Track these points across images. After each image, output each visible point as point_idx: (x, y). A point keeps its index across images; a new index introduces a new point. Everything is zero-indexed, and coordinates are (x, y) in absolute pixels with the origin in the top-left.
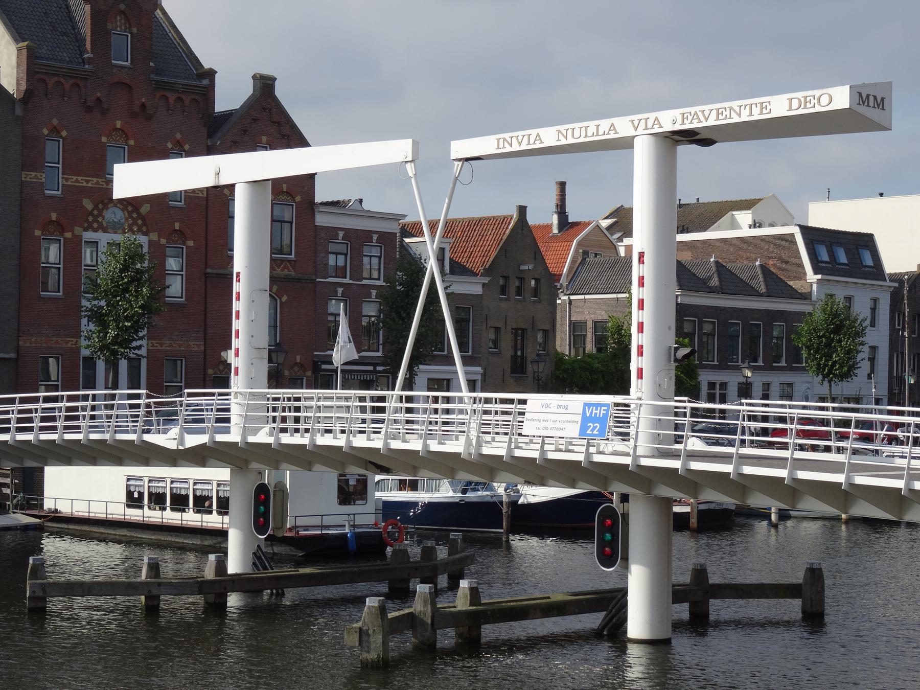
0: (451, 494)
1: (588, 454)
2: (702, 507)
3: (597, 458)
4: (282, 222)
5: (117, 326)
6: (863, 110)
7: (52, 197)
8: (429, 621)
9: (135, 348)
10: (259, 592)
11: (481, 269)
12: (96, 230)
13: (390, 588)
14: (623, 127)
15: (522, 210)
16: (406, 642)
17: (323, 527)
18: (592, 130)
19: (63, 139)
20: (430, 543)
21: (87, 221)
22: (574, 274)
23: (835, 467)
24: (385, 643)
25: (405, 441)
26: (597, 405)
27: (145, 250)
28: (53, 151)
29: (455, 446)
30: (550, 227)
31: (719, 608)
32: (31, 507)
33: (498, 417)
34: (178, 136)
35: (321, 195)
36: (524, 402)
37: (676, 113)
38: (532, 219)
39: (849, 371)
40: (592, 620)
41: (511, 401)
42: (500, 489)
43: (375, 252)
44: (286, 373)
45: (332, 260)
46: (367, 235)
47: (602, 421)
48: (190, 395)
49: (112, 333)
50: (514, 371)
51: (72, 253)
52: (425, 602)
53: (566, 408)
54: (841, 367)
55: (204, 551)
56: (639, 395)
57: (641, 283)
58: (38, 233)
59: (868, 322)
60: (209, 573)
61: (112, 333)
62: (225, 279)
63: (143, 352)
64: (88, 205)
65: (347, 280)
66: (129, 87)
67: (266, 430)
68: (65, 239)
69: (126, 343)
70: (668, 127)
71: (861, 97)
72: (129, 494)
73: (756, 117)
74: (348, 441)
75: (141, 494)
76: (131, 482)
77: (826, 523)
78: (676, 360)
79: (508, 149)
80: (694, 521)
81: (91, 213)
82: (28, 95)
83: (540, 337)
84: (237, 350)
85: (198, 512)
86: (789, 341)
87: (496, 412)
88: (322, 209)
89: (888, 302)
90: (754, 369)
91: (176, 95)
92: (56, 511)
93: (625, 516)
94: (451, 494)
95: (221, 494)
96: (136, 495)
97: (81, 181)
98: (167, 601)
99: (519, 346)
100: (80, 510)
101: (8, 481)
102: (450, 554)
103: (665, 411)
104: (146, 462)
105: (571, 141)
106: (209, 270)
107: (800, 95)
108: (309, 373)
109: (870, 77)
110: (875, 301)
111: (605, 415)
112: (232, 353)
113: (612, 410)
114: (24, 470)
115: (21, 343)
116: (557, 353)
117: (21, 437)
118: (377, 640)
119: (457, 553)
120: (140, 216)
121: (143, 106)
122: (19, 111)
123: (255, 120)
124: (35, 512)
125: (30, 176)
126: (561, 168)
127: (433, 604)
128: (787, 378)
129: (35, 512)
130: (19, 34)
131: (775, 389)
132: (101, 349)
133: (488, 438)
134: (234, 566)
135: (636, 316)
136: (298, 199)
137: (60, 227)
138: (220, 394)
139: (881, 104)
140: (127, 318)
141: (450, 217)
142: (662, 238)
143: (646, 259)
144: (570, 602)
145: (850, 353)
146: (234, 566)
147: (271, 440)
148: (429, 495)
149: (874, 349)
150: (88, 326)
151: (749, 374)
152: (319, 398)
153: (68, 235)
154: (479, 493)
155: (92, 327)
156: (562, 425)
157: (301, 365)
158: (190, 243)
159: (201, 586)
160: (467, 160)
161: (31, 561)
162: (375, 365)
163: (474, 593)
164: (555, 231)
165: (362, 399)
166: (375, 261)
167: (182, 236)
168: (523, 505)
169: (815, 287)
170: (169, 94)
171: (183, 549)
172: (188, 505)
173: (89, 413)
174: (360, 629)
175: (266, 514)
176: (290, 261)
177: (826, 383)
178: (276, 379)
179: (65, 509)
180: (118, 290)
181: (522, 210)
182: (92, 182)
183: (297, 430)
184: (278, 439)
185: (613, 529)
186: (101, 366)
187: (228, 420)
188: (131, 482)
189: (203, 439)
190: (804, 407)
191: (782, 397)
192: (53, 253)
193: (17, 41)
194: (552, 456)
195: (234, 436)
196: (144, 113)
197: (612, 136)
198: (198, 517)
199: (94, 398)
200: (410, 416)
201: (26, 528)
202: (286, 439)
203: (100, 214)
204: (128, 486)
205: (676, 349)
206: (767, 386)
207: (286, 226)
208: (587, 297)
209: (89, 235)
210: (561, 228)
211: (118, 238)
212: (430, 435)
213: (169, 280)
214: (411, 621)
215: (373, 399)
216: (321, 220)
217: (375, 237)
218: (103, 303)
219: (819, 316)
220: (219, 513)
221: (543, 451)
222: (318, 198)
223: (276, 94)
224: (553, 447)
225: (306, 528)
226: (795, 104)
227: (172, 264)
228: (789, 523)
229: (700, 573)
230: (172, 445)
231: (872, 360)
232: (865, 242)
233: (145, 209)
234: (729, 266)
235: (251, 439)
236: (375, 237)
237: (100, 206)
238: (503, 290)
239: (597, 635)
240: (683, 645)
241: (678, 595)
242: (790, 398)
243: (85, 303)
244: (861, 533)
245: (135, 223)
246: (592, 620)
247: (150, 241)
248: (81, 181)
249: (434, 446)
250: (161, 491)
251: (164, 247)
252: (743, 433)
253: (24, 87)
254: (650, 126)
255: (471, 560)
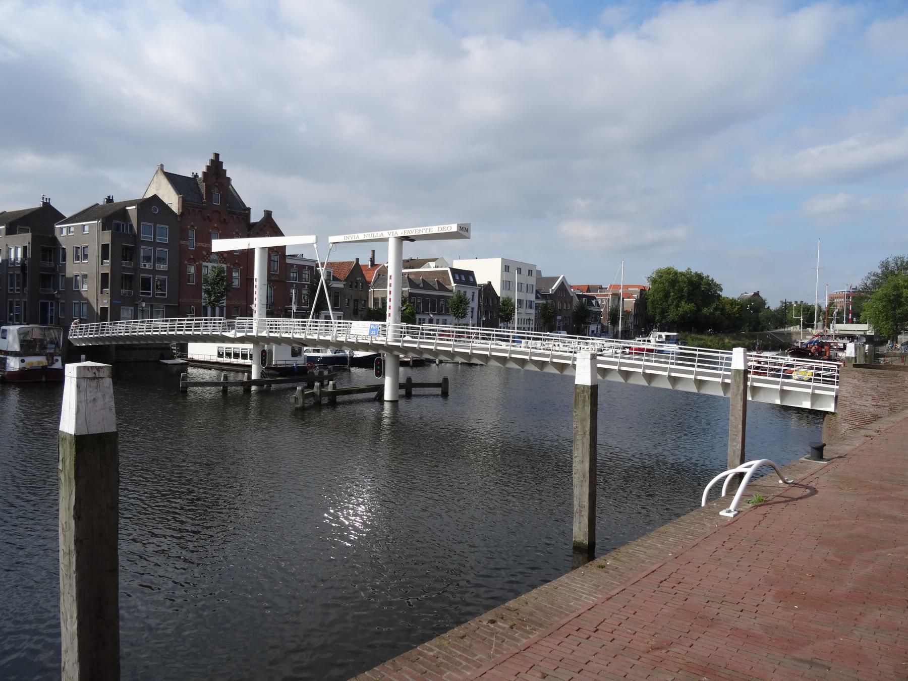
0: (331, 354)
1: (372, 341)
2: (414, 359)
3: (374, 342)
4: (274, 261)
5: (215, 296)
6: (461, 232)
7: (191, 250)
8: (319, 394)
9: (221, 303)
10: (263, 386)
11: (343, 279)
12: (207, 262)
13: (308, 384)
14: (385, 234)
15: (357, 260)
16: (312, 401)
17: (286, 364)
18: (375, 235)
19: (196, 230)
20: (321, 370)
21: (204, 259)
22: (375, 281)
23: (449, 346)
24: (303, 402)
25: (312, 336)
26: (374, 325)
27: (225, 269)
28: (192, 234)
29: (328, 338)
30: (368, 265)
31: (414, 391)
32: (183, 357)
33: (343, 328)
34: (237, 230)
35: (287, 253)
36: (351, 323)
37: (403, 230)
38: (361, 263)
39: (464, 315)
40: (373, 395)
41: (347, 323)
42: (347, 352)
43: (307, 272)
44: (275, 313)
45: (292, 275)
46: (304, 266)
47: (376, 330)
48: (238, 319)
49: (213, 298)
50: (354, 313)
51: (199, 270)
52: (317, 389)
53: (365, 326)
54: (462, 314)
55: (243, 372)
56: (389, 322)
57: (390, 286)
58: (186, 262)
59: (471, 300)
60: (245, 379)
61: (213, 298)
62: (251, 280)
63: (224, 304)
64: (204, 253)
65: (297, 282)
66: (219, 213)
67: (265, 332)
68: (196, 265)
69: (218, 301)
70: (400, 235)
71: (461, 228)
72: (219, 353)
73: (428, 233)
74: (280, 335)
75: (223, 353)
76: (219, 349)
77: (454, 364)
78: (401, 311)
79: (348, 240)
80: (411, 363)
81: (205, 256)
82: (182, 214)
83: (363, 302)
84: (255, 305)
85: (243, 359)
86: (445, 305)
87: (343, 327)
88: (288, 257)
89: (478, 293)
90: (433, 314)
91: (237, 216)
92: (192, 358)
93: (384, 361)
94: (331, 354)
95: (251, 353)
96: (221, 353)
97: (202, 245)
98: (231, 389)
99: (356, 305)
100: (201, 358)
101: (175, 348)
102: (328, 373)
103: (398, 327)
104: (223, 342)
105: (368, 238)
106: (248, 277)
107: (442, 226)
108: (283, 313)
109: (464, 221)
110: (473, 293)
111: (377, 328)
112: (254, 306)
113: (380, 327)
114: (181, 344)
115: (180, 301)
116: (369, 308)
117: (187, 333)
118: (301, 400)
119: (331, 373)
120: (223, 258)
121: (224, 219)
122: (179, 219)
123: (265, 226)
124: (185, 359)
125: (183, 242)
126: (373, 246)
127: (320, 389)
128: (445, 317)
129: (185, 359)
130: (179, 192)
131: (441, 321)
132: (209, 303)
133: (340, 335)
134: (254, 376)
135: (389, 296)
136: (280, 254)
137: (194, 261)
138: (249, 319)
139: (467, 230)
140: (219, 293)
141: (328, 261)
142: (398, 270)
143: (392, 278)
144: (367, 388)
145: (465, 310)
146: (254, 376)
147: (266, 335)
148: (323, 354)
149: (473, 308)
150: (204, 295)
151: (432, 316)
152: (284, 321)
153: (197, 263)
154: (340, 354)
155: (206, 296)
156: (363, 331)
157: (280, 310)
158: (242, 267)
159: (242, 383)
160: (334, 243)
161: (182, 375)
162: (306, 311)
163: (334, 385)
164: (370, 267)
165: (299, 322)
166: (307, 275)
167: (239, 265)
168: (355, 358)
169: (454, 288)
170: (234, 216)
171: (238, 372)
172: (239, 357)
173: (212, 325)
174: (295, 397)
175: (265, 360)
176: (277, 275)
177: (457, 319)
178: (270, 314)
179: (196, 358)
180: (215, 283)
181: (357, 260)
182: (206, 245)
183: (276, 332)
184: (269, 335)
185: (380, 365)
186: (209, 309)
187: (252, 328)
188: (219, 349)
189: (243, 334)
190: (443, 327)
191: (443, 324)
192: (192, 270)
193: (178, 195)
194: (359, 341)
195: (254, 334)
196: (225, 222)
197: (382, 237)
198: (243, 360)
199: (215, 320)
200: (327, 328)
201: (182, 364)
202: (272, 335)
203: (209, 256)
204: (218, 350)
205: (401, 307)
206: (438, 320)
207: (276, 263)
208: (379, 289)
209: (205, 264)
210: (371, 266)
211: (215, 265)
212: (321, 334)
213: (234, 280)
214: (313, 394)
215: (302, 322)
216: (288, 261)
217: (307, 267)
218: (210, 287)
219: (455, 297)
220: (250, 359)
221: (357, 340)
222: (287, 254)
223: (273, 217)
224: (374, 339)
225: (280, 365)
226: (440, 229)
227: (235, 274)
228: (443, 364)
229: (409, 380)
230: (232, 336)
231: (472, 312)
232: (470, 274)
233: (225, 255)
234: (426, 280)
235: (260, 335)
236: (307, 267)
237: (209, 254)
238: (351, 286)
239: (374, 400)
240: (402, 403)
241: (401, 386)
242: (445, 324)
243: (203, 287)
244: (465, 367)
245: (222, 260)
246: (373, 395)
247: (227, 266)
248: (202, 245)
249: (322, 338)
250: (230, 352)
251: (232, 268)
252: (493, 336)
253: (181, 211)
254: (394, 234)
255: (336, 375)
